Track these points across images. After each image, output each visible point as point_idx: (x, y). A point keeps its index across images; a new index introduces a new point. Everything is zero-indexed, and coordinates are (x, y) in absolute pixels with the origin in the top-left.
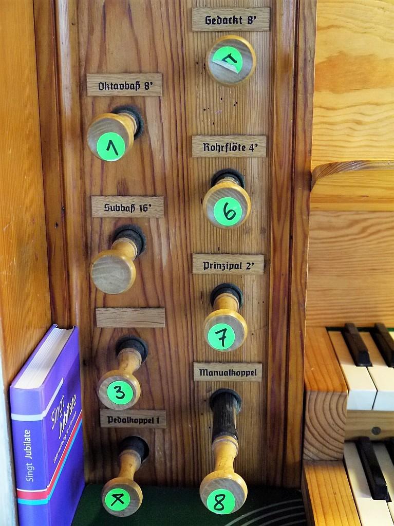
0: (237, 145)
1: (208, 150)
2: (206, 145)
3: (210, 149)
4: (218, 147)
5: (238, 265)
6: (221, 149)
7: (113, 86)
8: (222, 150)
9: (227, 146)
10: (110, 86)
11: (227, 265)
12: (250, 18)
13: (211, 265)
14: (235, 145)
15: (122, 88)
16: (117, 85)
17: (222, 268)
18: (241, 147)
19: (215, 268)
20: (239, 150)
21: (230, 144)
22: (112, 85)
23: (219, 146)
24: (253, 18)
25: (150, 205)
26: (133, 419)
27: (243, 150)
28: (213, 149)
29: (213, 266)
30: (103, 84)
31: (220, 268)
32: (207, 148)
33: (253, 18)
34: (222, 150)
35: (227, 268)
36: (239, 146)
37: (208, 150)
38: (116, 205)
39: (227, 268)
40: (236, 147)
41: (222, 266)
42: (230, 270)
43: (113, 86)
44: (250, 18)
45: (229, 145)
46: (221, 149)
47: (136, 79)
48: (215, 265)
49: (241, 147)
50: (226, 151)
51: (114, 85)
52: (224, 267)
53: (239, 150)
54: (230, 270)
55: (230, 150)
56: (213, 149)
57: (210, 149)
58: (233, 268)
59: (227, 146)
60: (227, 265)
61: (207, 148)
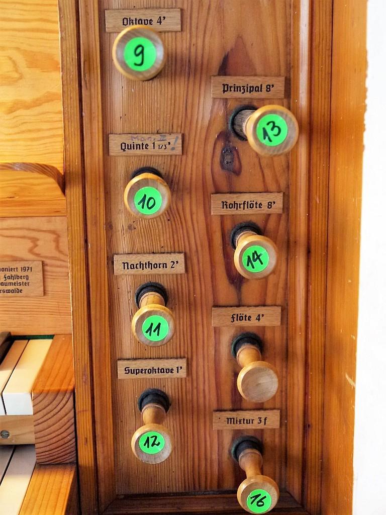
0: (254, 203)
1: (227, 208)
2: (225, 203)
3: (228, 207)
4: (236, 205)
5: (258, 87)
6: (238, 207)
7: (160, 370)
8: (240, 208)
9: (244, 204)
10: (157, 370)
11: (247, 88)
12: (270, 204)
13: (230, 87)
14: (242, 315)
15: (146, 23)
16: (164, 369)
17: (242, 91)
18: (247, 318)
19: (235, 91)
20: (246, 320)
21: (248, 202)
22: (136, 20)
23: (237, 204)
24: (273, 203)
25: (177, 262)
26: (151, 264)
27: (249, 320)
28: (231, 207)
29: (232, 89)
30: (127, 19)
31: (240, 91)
32: (225, 206)
33: (273, 203)
34: (240, 208)
35: (247, 91)
36: (256, 203)
37: (227, 208)
38: (149, 262)
39: (247, 91)
40: (253, 204)
41: (242, 88)
42: (250, 93)
43: (160, 370)
44: (270, 204)
45: (246, 203)
46: (238, 207)
47: (159, 15)
48: (235, 87)
49: (247, 318)
50: (244, 209)
51: (139, 21)
52: (244, 90)
53: (246, 320)
54: (250, 93)
55: (248, 208)
56: (231, 207)
57: (228, 207)
58: (253, 91)
59: (244, 204)
60: (247, 88)
61: (225, 206)
